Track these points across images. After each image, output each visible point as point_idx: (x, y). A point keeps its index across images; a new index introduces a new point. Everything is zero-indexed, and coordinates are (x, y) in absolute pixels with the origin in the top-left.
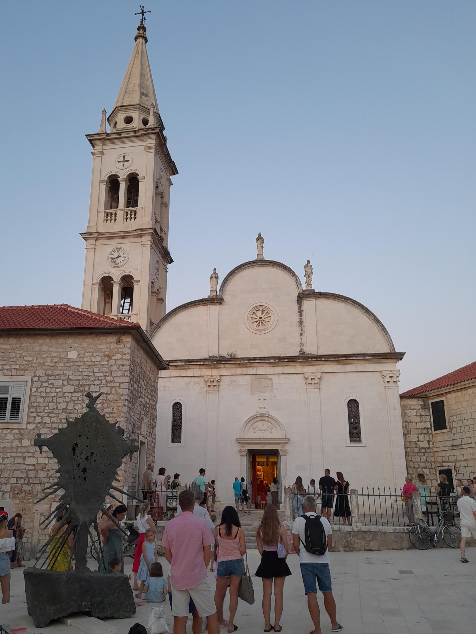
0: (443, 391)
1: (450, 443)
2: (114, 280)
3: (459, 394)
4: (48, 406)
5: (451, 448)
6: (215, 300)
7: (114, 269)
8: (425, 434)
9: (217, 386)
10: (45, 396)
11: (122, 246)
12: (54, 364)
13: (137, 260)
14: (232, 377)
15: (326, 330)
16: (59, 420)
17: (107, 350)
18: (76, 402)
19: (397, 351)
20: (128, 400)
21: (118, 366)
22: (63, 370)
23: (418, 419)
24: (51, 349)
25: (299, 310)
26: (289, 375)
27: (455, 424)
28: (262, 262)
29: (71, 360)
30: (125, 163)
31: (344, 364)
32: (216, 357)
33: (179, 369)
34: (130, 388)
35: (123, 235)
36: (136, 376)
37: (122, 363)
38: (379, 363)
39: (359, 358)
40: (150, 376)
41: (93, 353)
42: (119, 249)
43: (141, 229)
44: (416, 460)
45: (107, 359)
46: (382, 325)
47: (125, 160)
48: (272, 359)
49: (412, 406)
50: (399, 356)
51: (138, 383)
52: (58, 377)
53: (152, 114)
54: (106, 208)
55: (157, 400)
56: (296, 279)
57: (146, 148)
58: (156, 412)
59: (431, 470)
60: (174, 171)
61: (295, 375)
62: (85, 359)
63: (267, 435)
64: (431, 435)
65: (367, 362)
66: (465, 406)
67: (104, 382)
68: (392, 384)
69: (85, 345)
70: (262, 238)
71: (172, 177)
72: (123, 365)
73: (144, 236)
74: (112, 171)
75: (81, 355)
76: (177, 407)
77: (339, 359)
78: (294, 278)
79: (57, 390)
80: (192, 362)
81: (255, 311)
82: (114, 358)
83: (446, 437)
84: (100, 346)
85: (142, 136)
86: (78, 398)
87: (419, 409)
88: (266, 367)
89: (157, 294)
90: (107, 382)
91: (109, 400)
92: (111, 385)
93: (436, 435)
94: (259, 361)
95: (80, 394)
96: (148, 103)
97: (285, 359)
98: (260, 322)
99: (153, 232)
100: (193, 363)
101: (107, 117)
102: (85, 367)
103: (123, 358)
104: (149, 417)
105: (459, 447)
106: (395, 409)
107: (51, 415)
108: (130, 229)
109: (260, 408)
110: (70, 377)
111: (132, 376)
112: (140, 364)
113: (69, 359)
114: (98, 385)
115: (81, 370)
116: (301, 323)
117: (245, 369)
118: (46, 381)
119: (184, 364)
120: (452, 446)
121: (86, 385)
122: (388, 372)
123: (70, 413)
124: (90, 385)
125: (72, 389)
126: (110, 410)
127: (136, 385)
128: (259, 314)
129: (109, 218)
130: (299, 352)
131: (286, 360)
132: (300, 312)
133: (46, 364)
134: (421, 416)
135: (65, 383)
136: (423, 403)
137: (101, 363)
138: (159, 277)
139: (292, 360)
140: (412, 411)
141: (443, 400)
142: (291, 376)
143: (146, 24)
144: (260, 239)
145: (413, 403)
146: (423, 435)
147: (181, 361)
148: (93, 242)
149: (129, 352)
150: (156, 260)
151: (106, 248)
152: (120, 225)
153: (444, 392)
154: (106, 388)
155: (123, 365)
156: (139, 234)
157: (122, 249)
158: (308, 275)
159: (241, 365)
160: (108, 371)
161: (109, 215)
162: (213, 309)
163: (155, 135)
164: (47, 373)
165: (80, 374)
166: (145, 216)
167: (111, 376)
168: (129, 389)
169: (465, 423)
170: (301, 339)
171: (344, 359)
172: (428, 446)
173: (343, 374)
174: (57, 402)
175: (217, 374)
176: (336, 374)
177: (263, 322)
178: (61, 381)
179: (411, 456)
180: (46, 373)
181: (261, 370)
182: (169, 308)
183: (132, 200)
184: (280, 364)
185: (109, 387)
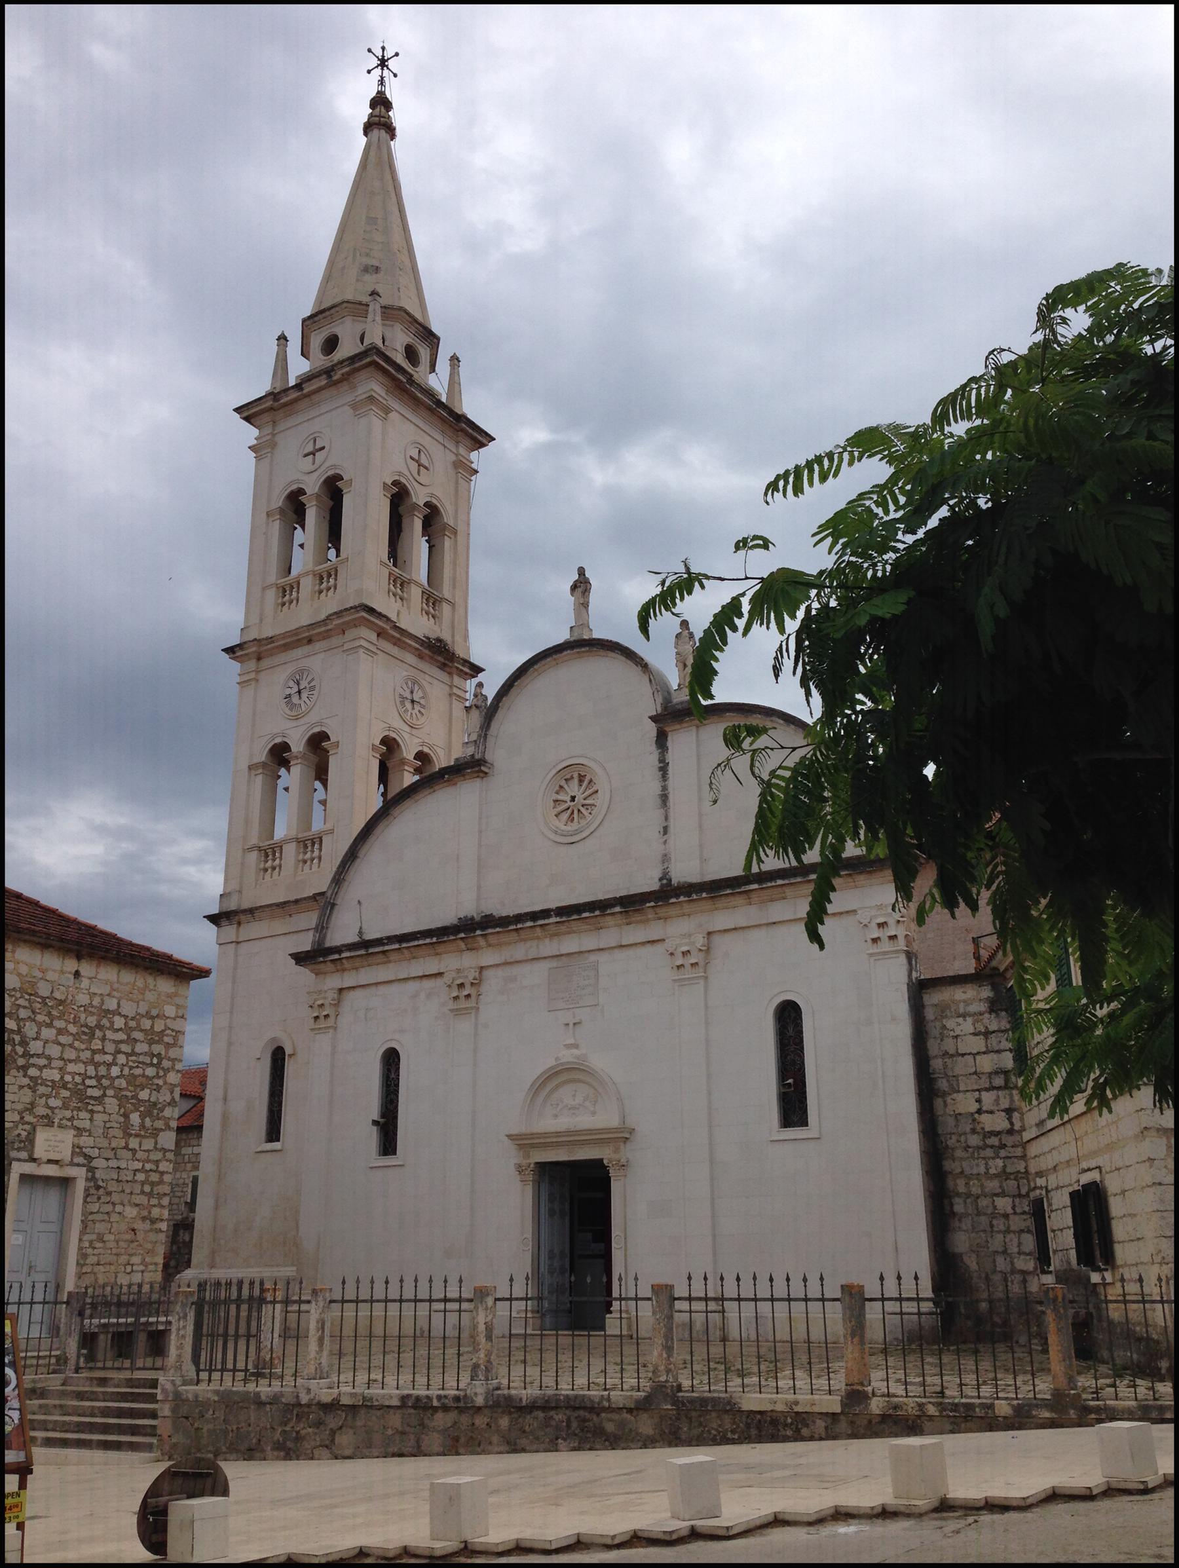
8: (999, 1088)
9: (473, 997)
23: (978, 1044)
31: (763, 902)
32: (472, 918)
35: (323, 629)
42: (301, 672)
44: (975, 1171)
57: (355, 406)
59: (1017, 1200)
60: (479, 438)
63: (584, 1121)
77: (743, 889)
78: (634, 671)
85: (345, 378)
87: (981, 1014)
97: (613, 906)
98: (572, 811)
100: (416, 943)
106: (894, 1019)
116: (664, 798)
122: (873, 913)
128: (573, 788)
130: (661, 879)
131: (618, 909)
132: (664, 769)
134: (987, 1034)
136: (991, 994)
140: (960, 1020)
143: (393, 93)
145: (964, 997)
148: (252, 664)
151: (277, 678)
170: (665, 842)
176: (381, 988)
177: (583, 810)
179: (962, 1159)
181: (570, 944)
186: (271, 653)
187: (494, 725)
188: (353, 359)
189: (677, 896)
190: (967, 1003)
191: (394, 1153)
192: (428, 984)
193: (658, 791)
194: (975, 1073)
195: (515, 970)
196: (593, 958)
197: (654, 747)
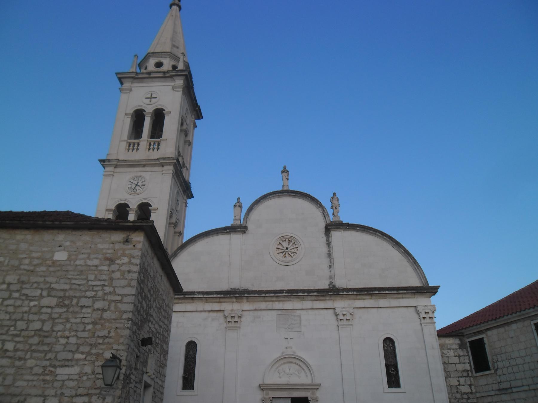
0: (483, 327)
1: (496, 387)
3: (501, 330)
4: (15, 326)
5: (498, 393)
6: (238, 229)
7: (132, 197)
9: (239, 322)
10: (12, 311)
11: (142, 174)
13: (157, 189)
14: (256, 312)
15: (358, 261)
16: (28, 347)
17: (109, 251)
18: (57, 321)
19: (431, 284)
20: (132, 320)
21: (123, 273)
22: (45, 276)
23: (456, 360)
24: (32, 248)
25: (327, 241)
27: (500, 365)
28: (288, 193)
29: (58, 263)
30: (153, 100)
33: (196, 303)
34: (137, 303)
36: (146, 290)
37: (127, 269)
38: (412, 298)
40: (164, 297)
41: (89, 254)
42: (138, 177)
43: (164, 159)
45: (108, 262)
46: (413, 257)
47: (153, 96)
48: (300, 293)
49: (449, 345)
50: (433, 290)
51: (148, 302)
52: (35, 285)
53: (181, 60)
54: (130, 137)
55: (170, 331)
56: (323, 210)
57: (174, 88)
58: (168, 347)
62: (78, 263)
63: (295, 380)
64: (471, 378)
65: (400, 296)
67: (100, 294)
68: (428, 320)
69: (79, 244)
70: (288, 171)
71: (197, 122)
72: (129, 272)
75: (73, 257)
76: (191, 347)
77: (372, 293)
78: (320, 209)
79: (32, 304)
80: (211, 294)
81: (281, 242)
82: (118, 262)
83: (490, 380)
84: (100, 246)
86: (60, 315)
87: (456, 349)
88: (293, 301)
89: (175, 223)
90: (105, 294)
92: (110, 297)
93: (478, 378)
94: (287, 295)
96: (178, 53)
97: (314, 292)
98: (286, 252)
100: (212, 296)
101: (139, 62)
102: (76, 273)
103: (130, 263)
104: (159, 352)
105: (508, 391)
106: (433, 348)
107: (17, 339)
109: (287, 348)
110: (53, 286)
111: (141, 288)
112: (152, 276)
113: (54, 263)
114: (91, 297)
115: (70, 277)
116: (330, 255)
117: (270, 303)
118: (18, 291)
119: (201, 296)
120: (499, 390)
121: (75, 297)
124: (80, 297)
126: (105, 333)
127: (146, 302)
128: (285, 245)
129: (131, 147)
130: (329, 285)
131: (315, 294)
132: (329, 244)
133: (22, 267)
134: (459, 356)
135: (45, 293)
136: (459, 342)
137: (100, 268)
138: (178, 209)
139: (321, 294)
140: (449, 351)
142: (321, 311)
144: (285, 171)
146: (464, 378)
147: (199, 293)
148: (111, 169)
149: (140, 254)
151: (124, 177)
152: (143, 153)
155: (129, 272)
157: (142, 177)
158: (334, 207)
159: (266, 299)
160: (107, 278)
161: (132, 145)
162: (236, 238)
163: (184, 77)
164: (21, 280)
165: (68, 281)
166: (169, 144)
167: (111, 285)
168: (135, 305)
169: (513, 362)
171: (377, 292)
172: (469, 391)
173: (375, 310)
175: (239, 308)
176: (369, 309)
177: (290, 253)
180: (19, 280)
181: (288, 305)
182: (187, 237)
184: (309, 298)
186: (122, 166)
188: (164, 72)
189: (343, 292)
190: (452, 344)
191: (193, 389)
193: (327, 252)
195: (259, 313)
196: (298, 312)
197: (324, 235)
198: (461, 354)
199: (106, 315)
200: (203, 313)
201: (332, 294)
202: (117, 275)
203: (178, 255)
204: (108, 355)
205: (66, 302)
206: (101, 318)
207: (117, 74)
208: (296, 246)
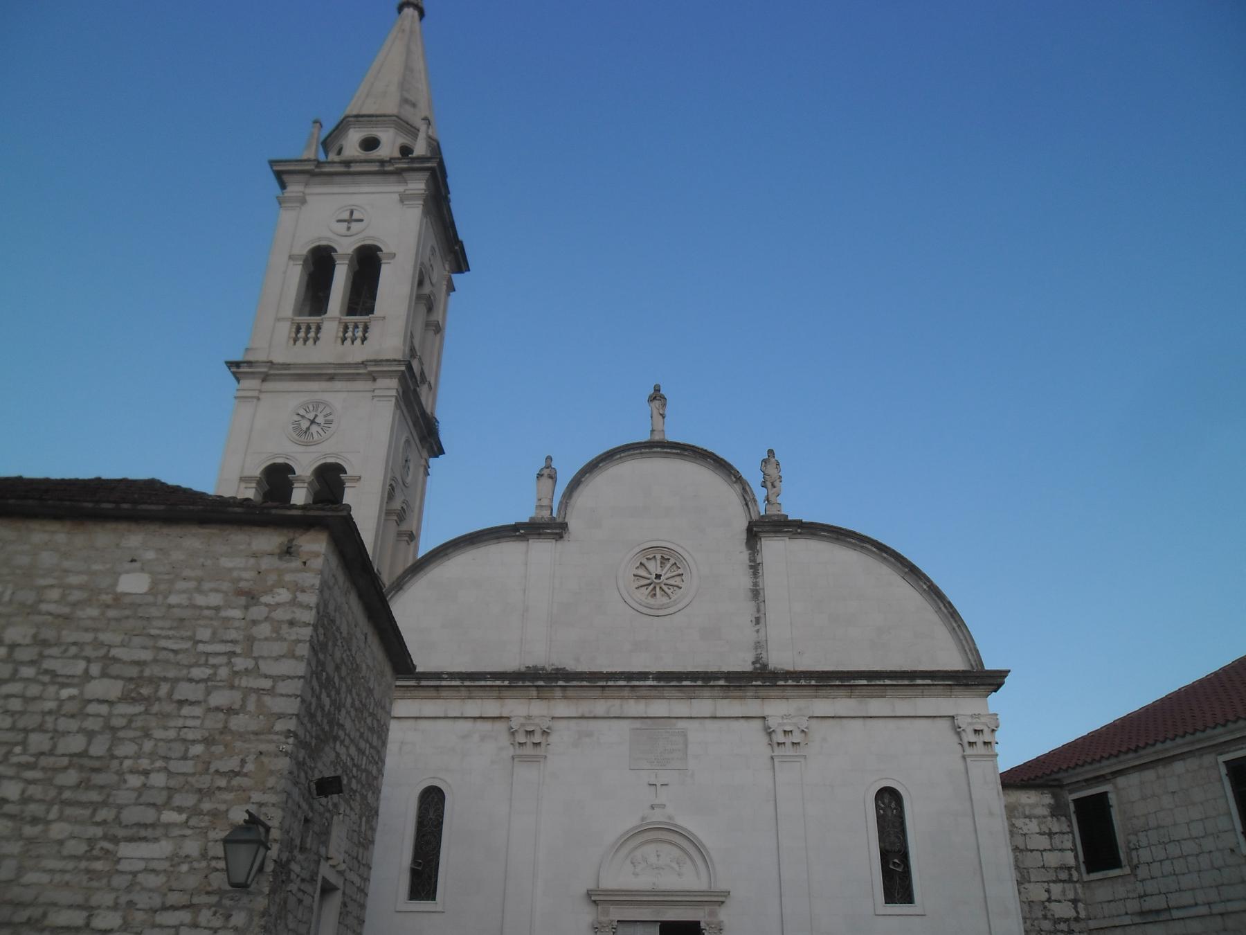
0: (1106, 768)
1: (1133, 906)
2: (298, 472)
3: (1150, 775)
4: (24, 743)
5: (1138, 920)
6: (546, 528)
8: (1064, 881)
9: (543, 745)
12: (66, 610)
13: (361, 435)
14: (583, 722)
15: (820, 609)
16: (52, 793)
17: (246, 575)
20: (296, 735)
21: (277, 625)
22: (96, 630)
23: (1044, 842)
24: (67, 564)
25: (751, 561)
26: (727, 721)
27: (1145, 855)
29: (127, 600)
31: (863, 697)
37: (288, 617)
39: (900, 682)
41: (200, 580)
42: (317, 404)
43: (377, 362)
45: (243, 600)
46: (950, 603)
48: (686, 679)
49: (1027, 809)
51: (333, 693)
53: (422, 135)
54: (299, 311)
57: (403, 199)
61: (742, 721)
62: (173, 600)
63: (669, 881)
64: (1078, 885)
66: (1170, 805)
67: (223, 672)
68: (980, 749)
69: (177, 556)
70: (663, 398)
71: (456, 278)
72: (292, 623)
73: (384, 377)
74: (320, 239)
75: (162, 587)
76: (432, 800)
77: (852, 682)
78: (737, 487)
79: (65, 693)
81: (644, 561)
82: (266, 599)
83: (1121, 891)
84: (226, 563)
85: (398, 172)
86: (130, 721)
87: (1045, 817)
90: (236, 673)
91: (232, 732)
92: (245, 682)
94: (655, 683)
95: (139, 708)
98: (655, 585)
99: (403, 368)
100: (483, 683)
102: (168, 624)
106: (991, 814)
107: (30, 774)
108: (350, 360)
109: (652, 807)
110: (114, 652)
112: (345, 634)
115: (153, 632)
116: (756, 593)
117: (617, 702)
118: (32, 663)
119: (458, 683)
120: (1142, 913)
121: (165, 679)
123: (94, 770)
124: (176, 680)
125: (113, 689)
126: (233, 764)
127: (329, 695)
128: (654, 567)
130: (754, 663)
131: (722, 683)
132: (755, 568)
133: (44, 607)
134: (1051, 834)
135: (95, 669)
136: (1052, 801)
137: (223, 614)
139: (735, 683)
140: (1027, 820)
141: (1106, 793)
144: (657, 396)
147: (452, 676)
150: (403, 440)
151: (287, 402)
152: (328, 348)
153: (1108, 771)
154: (227, 693)
155: (292, 623)
156: (370, 373)
159: (608, 693)
160: (240, 638)
162: (541, 549)
163: (427, 175)
166: (389, 328)
167: (248, 653)
168: (303, 701)
169: (1173, 850)
170: (758, 631)
171: (865, 682)
173: (860, 722)
174: (55, 731)
176: (844, 721)
177: (665, 588)
178: (82, 665)
181: (659, 708)
183: (363, 296)
185: (239, 688)
187: (576, 494)
188: (382, 162)
189: (786, 680)
190: (1032, 806)
192: (486, 726)
193: (750, 585)
194: (1043, 867)
196: (681, 724)
198: (1055, 829)
199: (237, 723)
200: (461, 723)
201: (759, 683)
202: (264, 630)
203: (405, 587)
204: (238, 816)
205: (145, 691)
206: (225, 730)
207: (272, 163)
208: (680, 571)
